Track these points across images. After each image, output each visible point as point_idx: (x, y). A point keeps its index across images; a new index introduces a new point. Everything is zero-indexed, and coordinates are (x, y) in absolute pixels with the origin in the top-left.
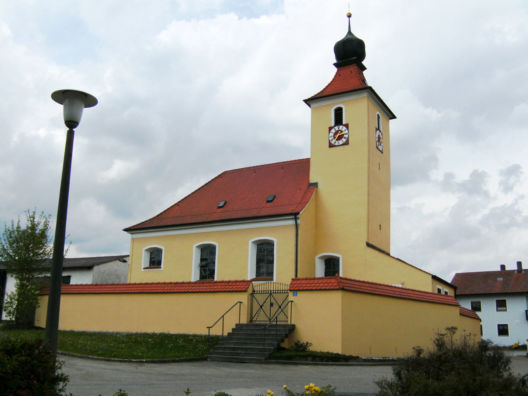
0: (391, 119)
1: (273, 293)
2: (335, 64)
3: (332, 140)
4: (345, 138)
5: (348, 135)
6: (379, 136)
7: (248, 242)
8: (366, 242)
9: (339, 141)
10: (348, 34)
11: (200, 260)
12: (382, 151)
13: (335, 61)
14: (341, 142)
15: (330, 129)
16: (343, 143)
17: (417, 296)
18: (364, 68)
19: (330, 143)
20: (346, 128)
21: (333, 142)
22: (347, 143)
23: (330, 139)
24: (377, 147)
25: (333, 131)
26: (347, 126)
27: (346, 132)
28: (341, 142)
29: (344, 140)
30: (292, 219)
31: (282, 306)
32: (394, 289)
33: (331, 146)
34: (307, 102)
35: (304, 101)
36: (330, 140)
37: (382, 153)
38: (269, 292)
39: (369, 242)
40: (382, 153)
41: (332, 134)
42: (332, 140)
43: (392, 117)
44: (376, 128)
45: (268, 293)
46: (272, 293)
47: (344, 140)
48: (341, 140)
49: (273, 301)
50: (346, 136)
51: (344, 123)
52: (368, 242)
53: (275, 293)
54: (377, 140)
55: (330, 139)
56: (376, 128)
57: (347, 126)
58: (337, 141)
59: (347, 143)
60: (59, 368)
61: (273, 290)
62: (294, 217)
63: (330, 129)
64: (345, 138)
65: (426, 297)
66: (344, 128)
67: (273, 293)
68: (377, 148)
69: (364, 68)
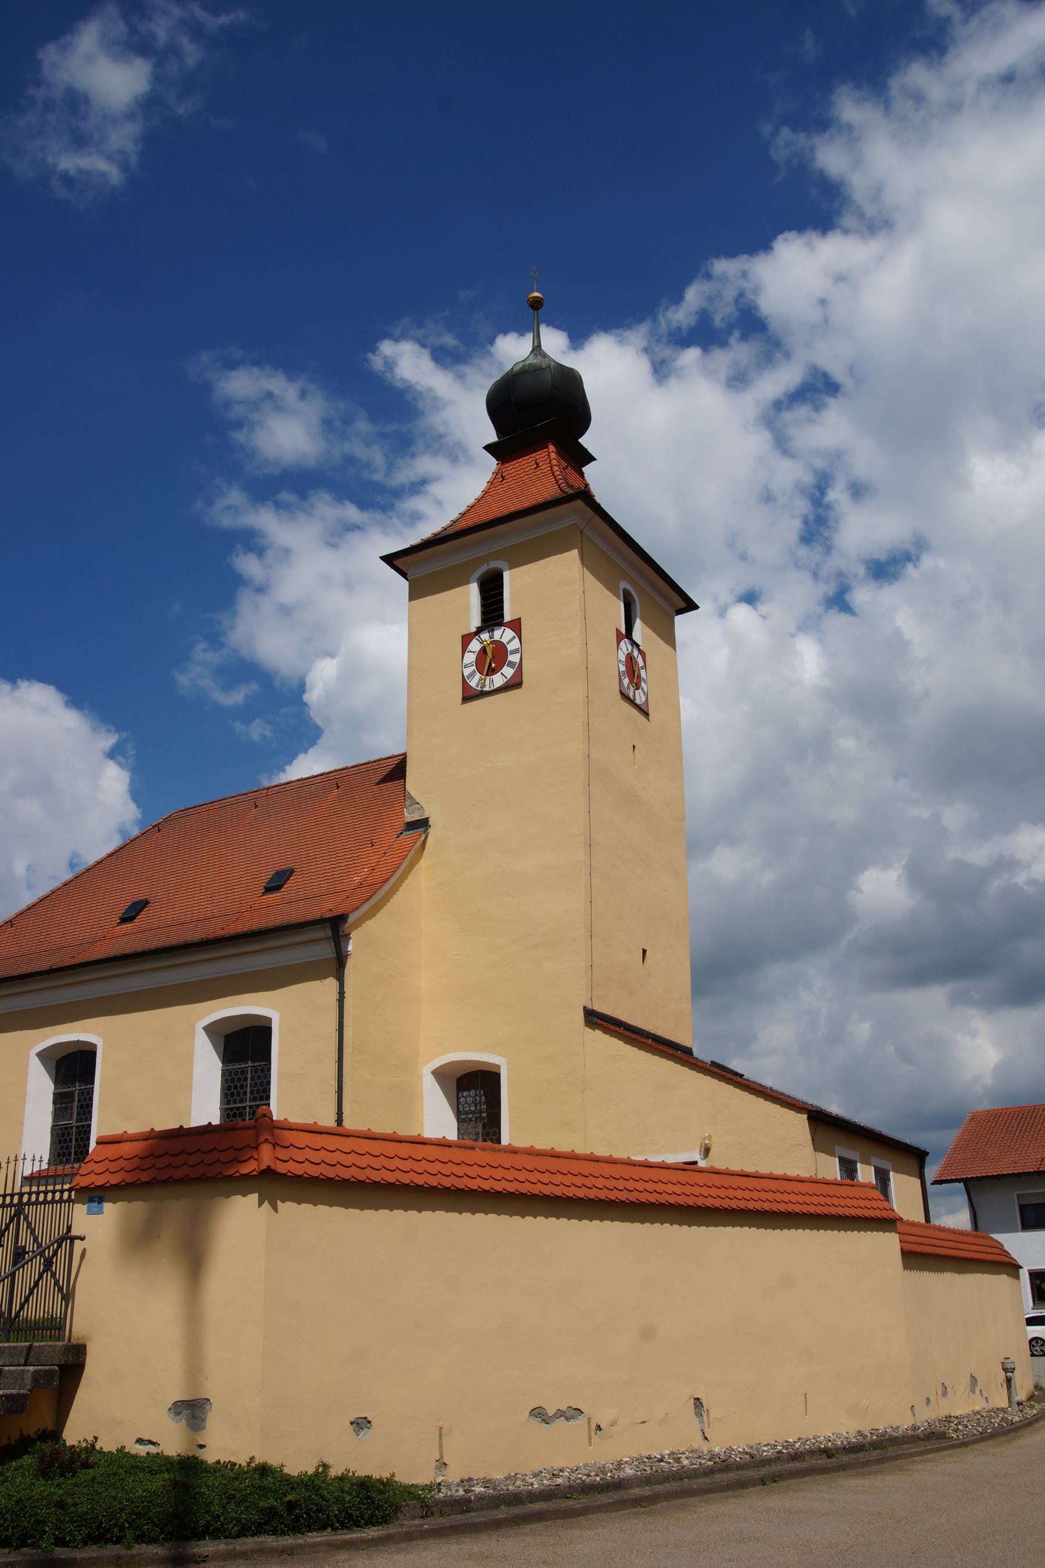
0: (680, 612)
1: (29, 1203)
2: (489, 448)
3: (472, 674)
4: (511, 664)
5: (519, 655)
6: (630, 658)
7: (193, 1027)
8: (584, 1007)
9: (494, 677)
10: (532, 355)
11: (51, 1097)
12: (643, 707)
13: (492, 437)
14: (498, 680)
15: (466, 640)
16: (505, 680)
17: (822, 1200)
18: (588, 458)
19: (465, 684)
20: (513, 634)
21: (473, 683)
22: (514, 684)
23: (467, 672)
24: (622, 693)
25: (475, 646)
26: (516, 626)
27: (515, 645)
28: (498, 680)
29: (508, 672)
30: (328, 938)
31: (54, 1260)
32: (656, 1174)
33: (470, 695)
34: (397, 562)
35: (384, 558)
36: (465, 675)
37: (646, 714)
38: (16, 1200)
39: (594, 1008)
40: (646, 714)
41: (470, 658)
42: (472, 674)
43: (682, 605)
44: (618, 631)
45: (11, 1205)
46: (25, 1204)
47: (508, 672)
48: (500, 673)
49: (25, 1239)
50: (514, 658)
51: (507, 617)
52: (589, 1007)
53: (37, 1203)
54: (623, 668)
55: (467, 672)
56: (618, 631)
57: (516, 626)
58: (488, 678)
59: (518, 681)
60: (368, 1428)
61: (11, 1192)
62: (329, 933)
63: (466, 640)
64: (511, 664)
65: (849, 1202)
66: (509, 633)
67: (29, 1203)
68: (625, 697)
69: (588, 458)
